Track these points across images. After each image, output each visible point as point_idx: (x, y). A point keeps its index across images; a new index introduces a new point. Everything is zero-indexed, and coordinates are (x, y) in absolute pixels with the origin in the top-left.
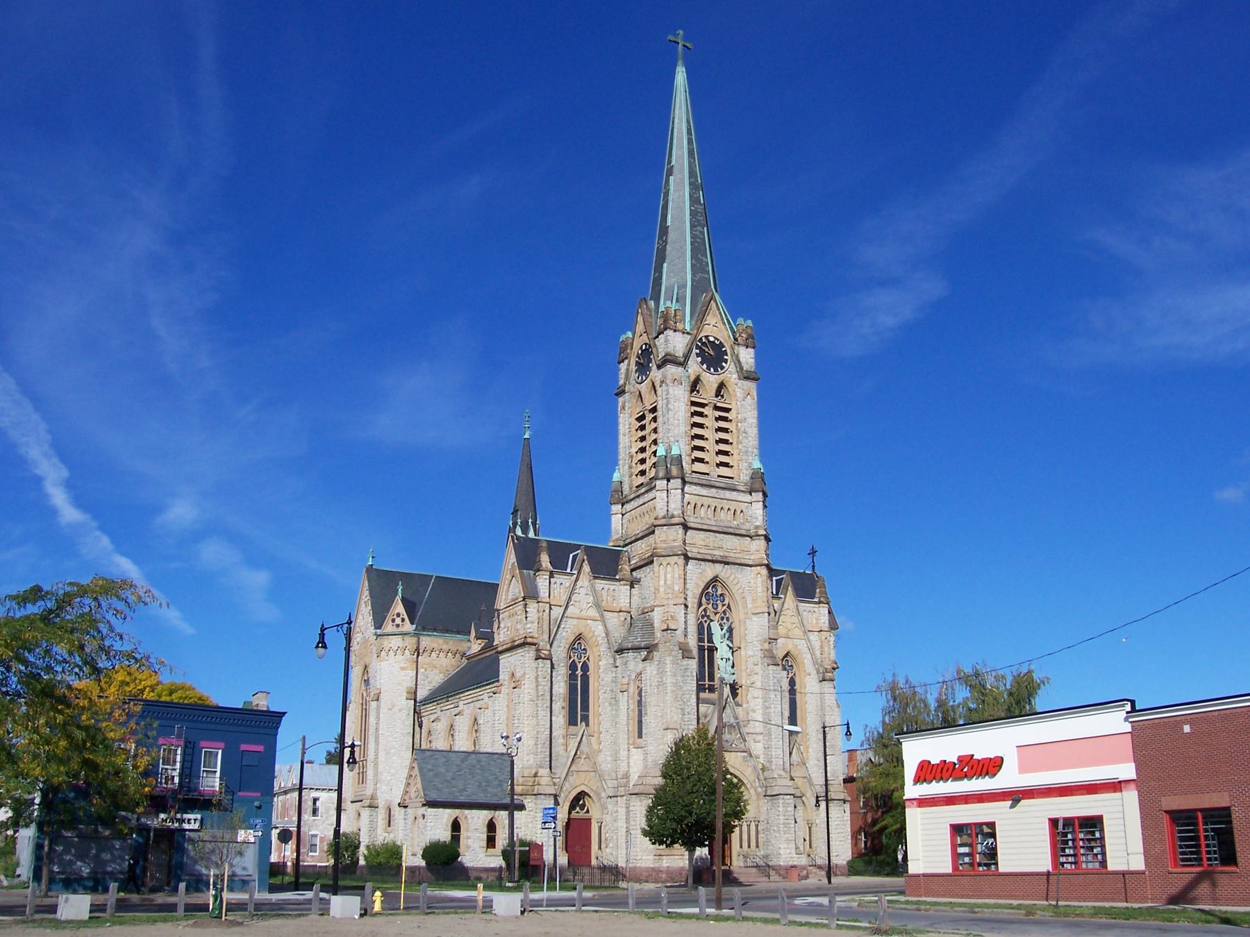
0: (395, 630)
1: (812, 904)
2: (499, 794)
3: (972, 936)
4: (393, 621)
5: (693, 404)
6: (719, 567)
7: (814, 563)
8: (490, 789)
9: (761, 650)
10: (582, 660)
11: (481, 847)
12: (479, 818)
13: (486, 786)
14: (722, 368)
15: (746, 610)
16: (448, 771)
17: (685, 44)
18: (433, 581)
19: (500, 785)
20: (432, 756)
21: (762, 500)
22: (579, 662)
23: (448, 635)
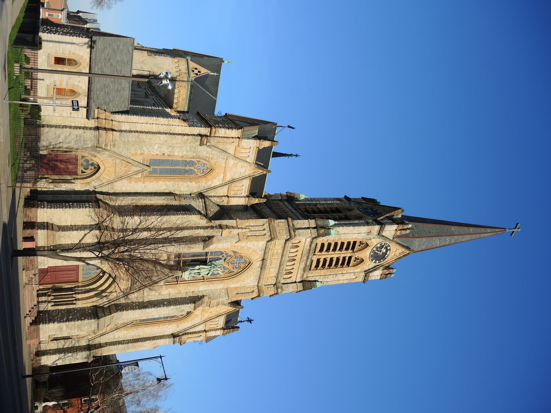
0: (190, 70)
1: (69, 174)
2: (99, 101)
4: (196, 69)
5: (355, 243)
6: (259, 264)
7: (244, 322)
8: (102, 93)
10: (196, 170)
11: (55, 82)
12: (79, 82)
13: (105, 91)
14: (372, 260)
16: (117, 62)
17: (515, 232)
18: (214, 98)
19: (105, 103)
20: (129, 51)
22: (195, 168)
23: (188, 101)
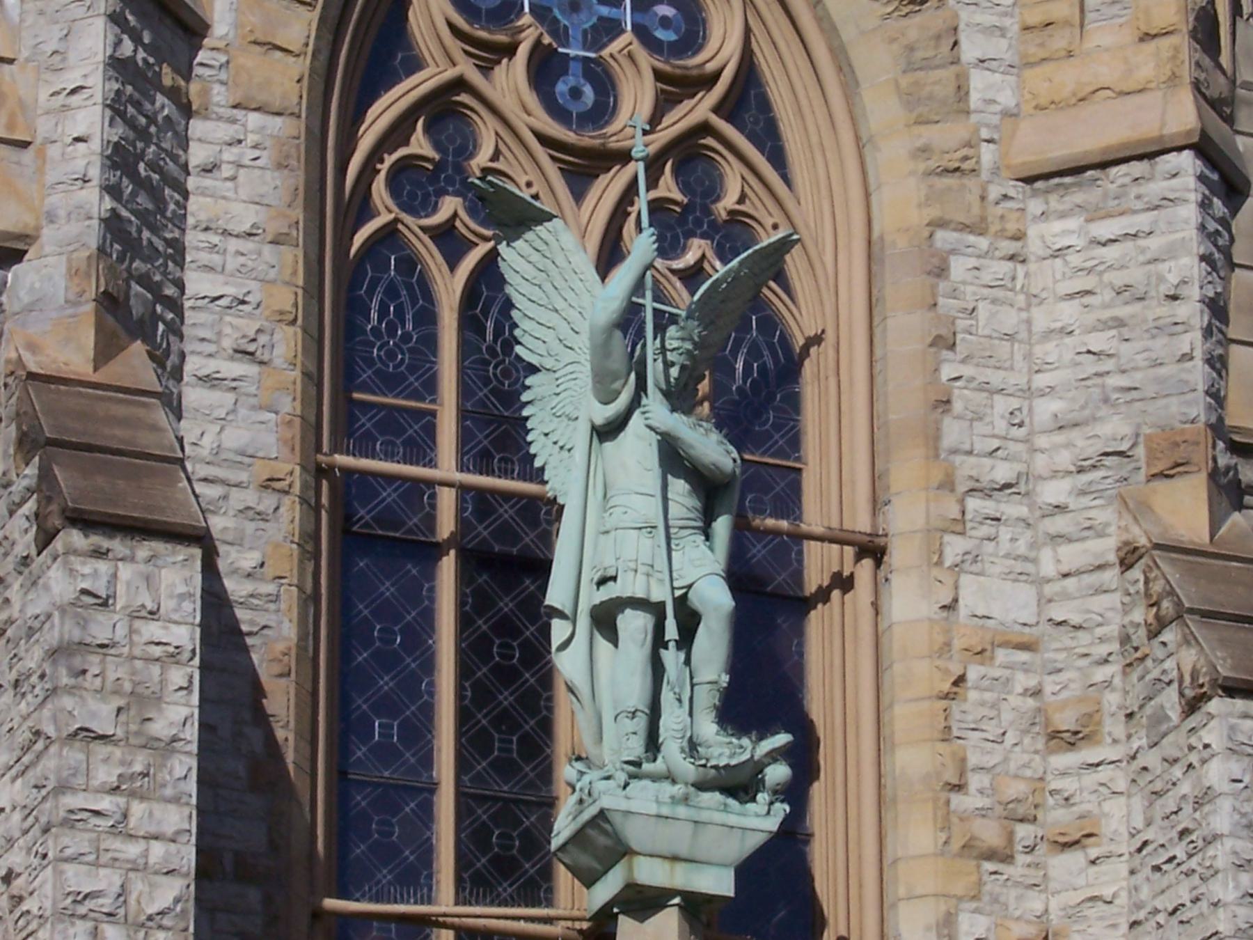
3: (668, 922)
9: (1129, 557)
15: (946, 135)
21: (969, 774)
